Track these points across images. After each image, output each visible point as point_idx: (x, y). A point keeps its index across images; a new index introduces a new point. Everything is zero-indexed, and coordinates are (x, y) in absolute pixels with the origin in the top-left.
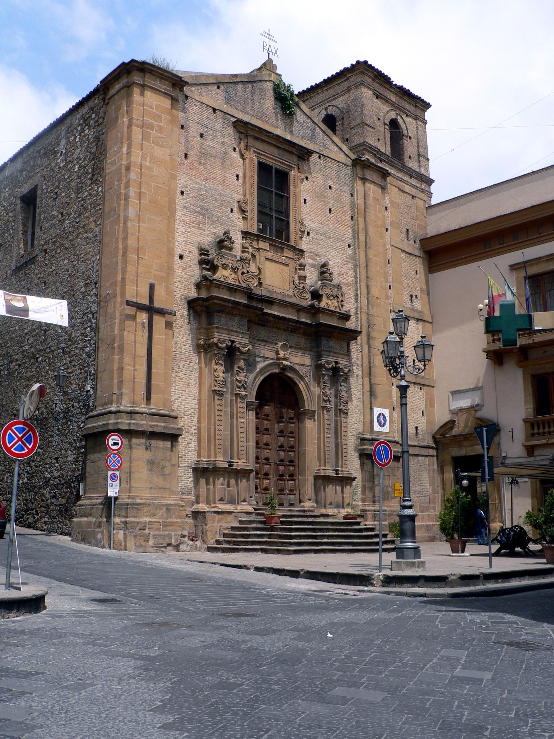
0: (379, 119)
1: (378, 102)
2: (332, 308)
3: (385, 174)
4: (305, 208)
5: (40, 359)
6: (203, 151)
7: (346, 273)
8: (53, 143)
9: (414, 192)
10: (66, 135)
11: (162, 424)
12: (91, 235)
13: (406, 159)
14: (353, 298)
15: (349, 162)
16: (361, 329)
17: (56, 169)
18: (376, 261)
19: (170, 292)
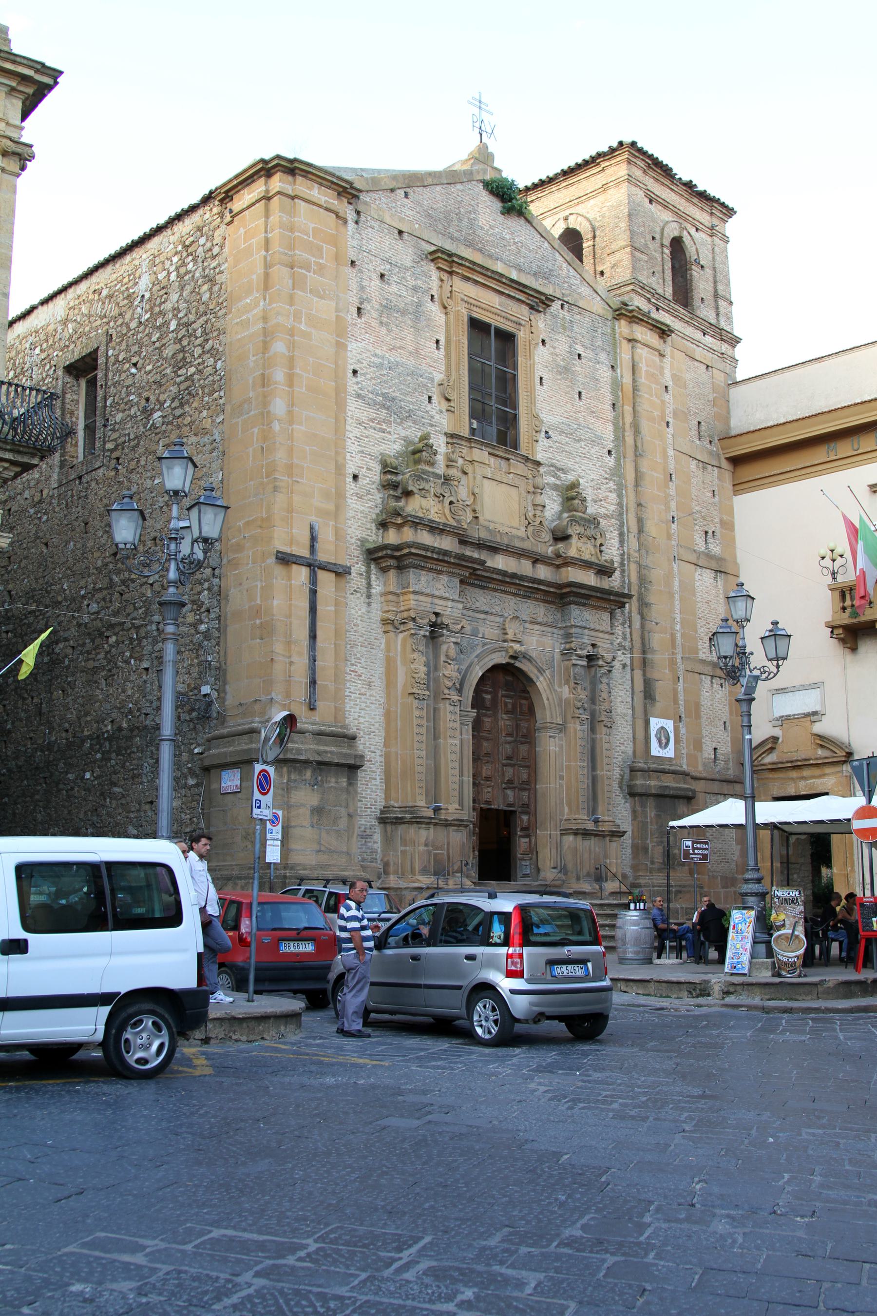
0: (654, 238)
3: (664, 332)
4: (541, 392)
5: (114, 638)
6: (384, 302)
8: (126, 280)
9: (709, 358)
10: (150, 268)
11: (333, 749)
12: (206, 439)
13: (697, 302)
14: (617, 539)
16: (629, 589)
18: (653, 475)
19: (339, 535)
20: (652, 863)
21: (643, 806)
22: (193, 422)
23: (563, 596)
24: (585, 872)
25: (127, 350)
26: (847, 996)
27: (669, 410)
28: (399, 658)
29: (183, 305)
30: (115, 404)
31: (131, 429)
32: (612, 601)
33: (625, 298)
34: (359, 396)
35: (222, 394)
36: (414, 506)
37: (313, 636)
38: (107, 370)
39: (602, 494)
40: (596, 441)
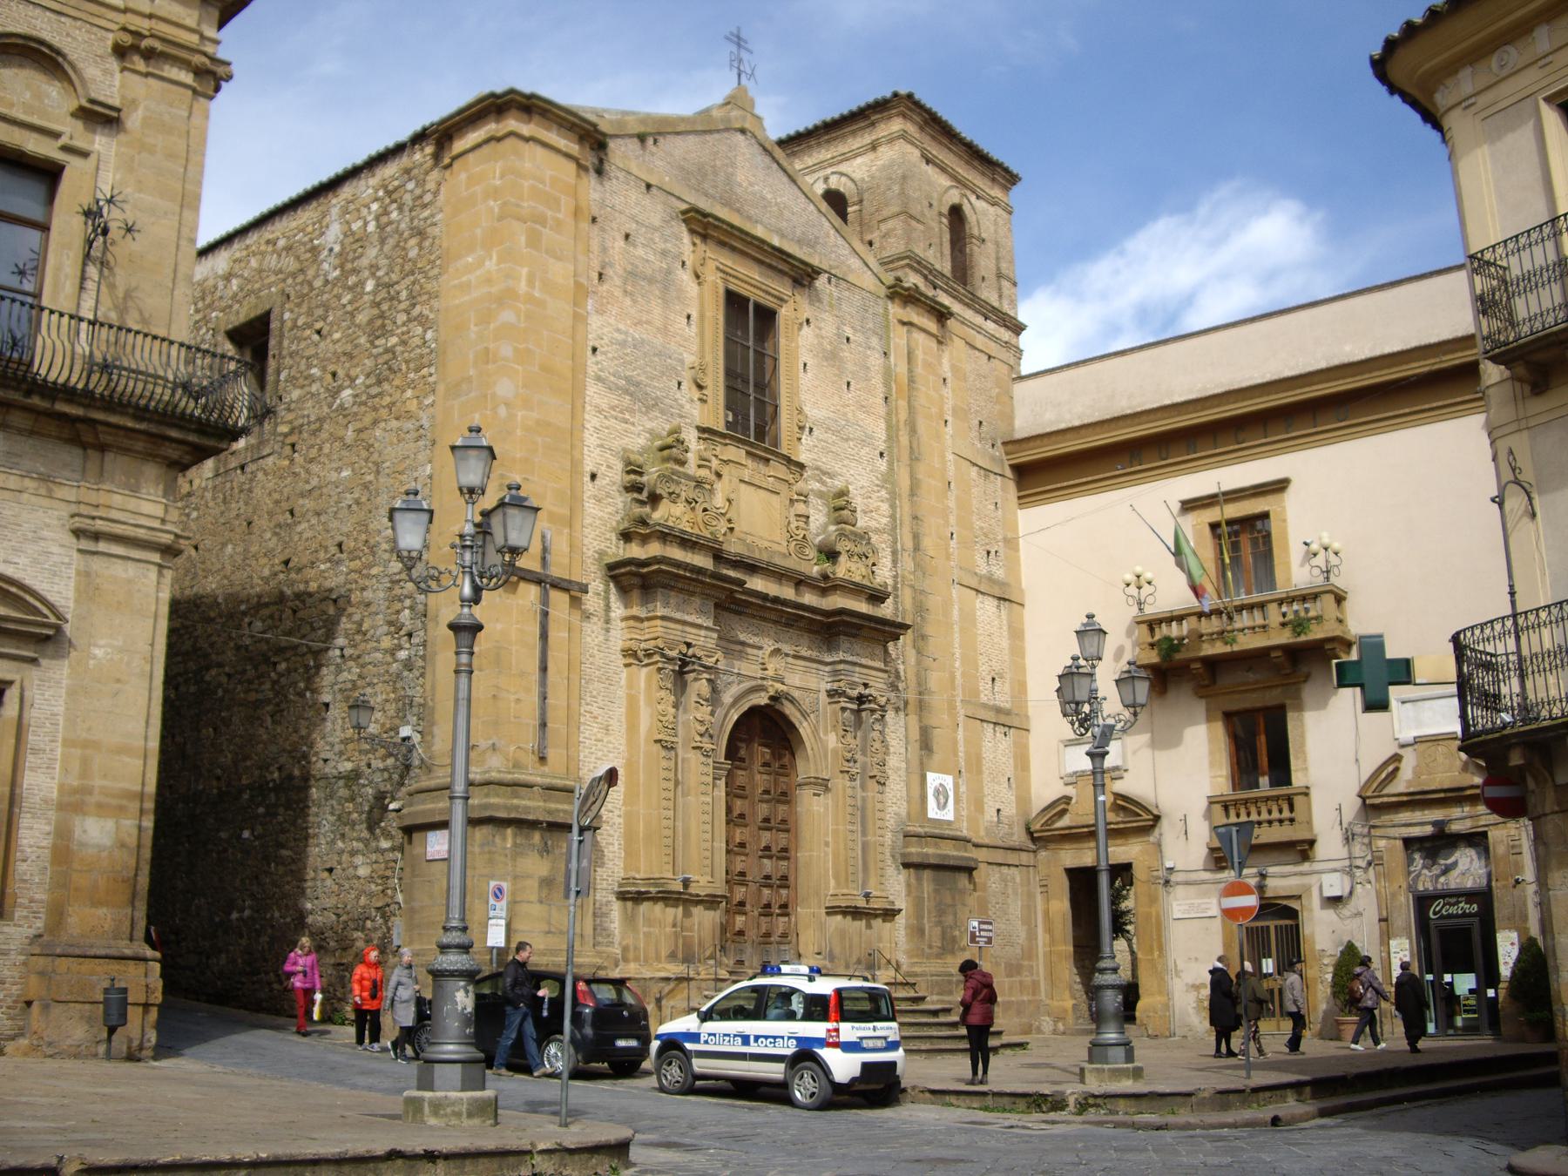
1: (930, 169)
2: (857, 579)
3: (942, 315)
4: (805, 380)
6: (629, 268)
7: (877, 509)
8: (310, 229)
9: (993, 348)
12: (409, 425)
13: (977, 281)
15: (883, 291)
17: (318, 283)
20: (930, 947)
21: (919, 879)
22: (393, 404)
23: (831, 630)
24: (854, 959)
25: (310, 313)
26: (1225, 1107)
27: (948, 406)
28: (642, 697)
29: (383, 262)
30: (291, 379)
31: (311, 410)
32: (888, 631)
33: (899, 273)
34: (599, 379)
35: (432, 370)
36: (662, 514)
37: (544, 669)
38: (282, 336)
39: (874, 503)
40: (866, 440)
